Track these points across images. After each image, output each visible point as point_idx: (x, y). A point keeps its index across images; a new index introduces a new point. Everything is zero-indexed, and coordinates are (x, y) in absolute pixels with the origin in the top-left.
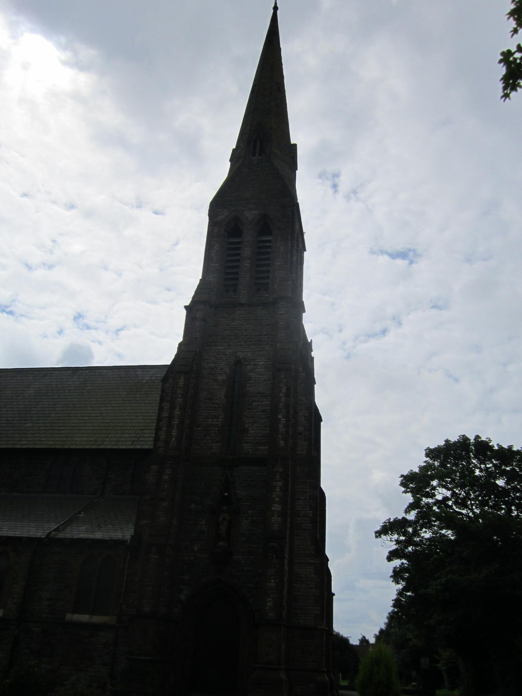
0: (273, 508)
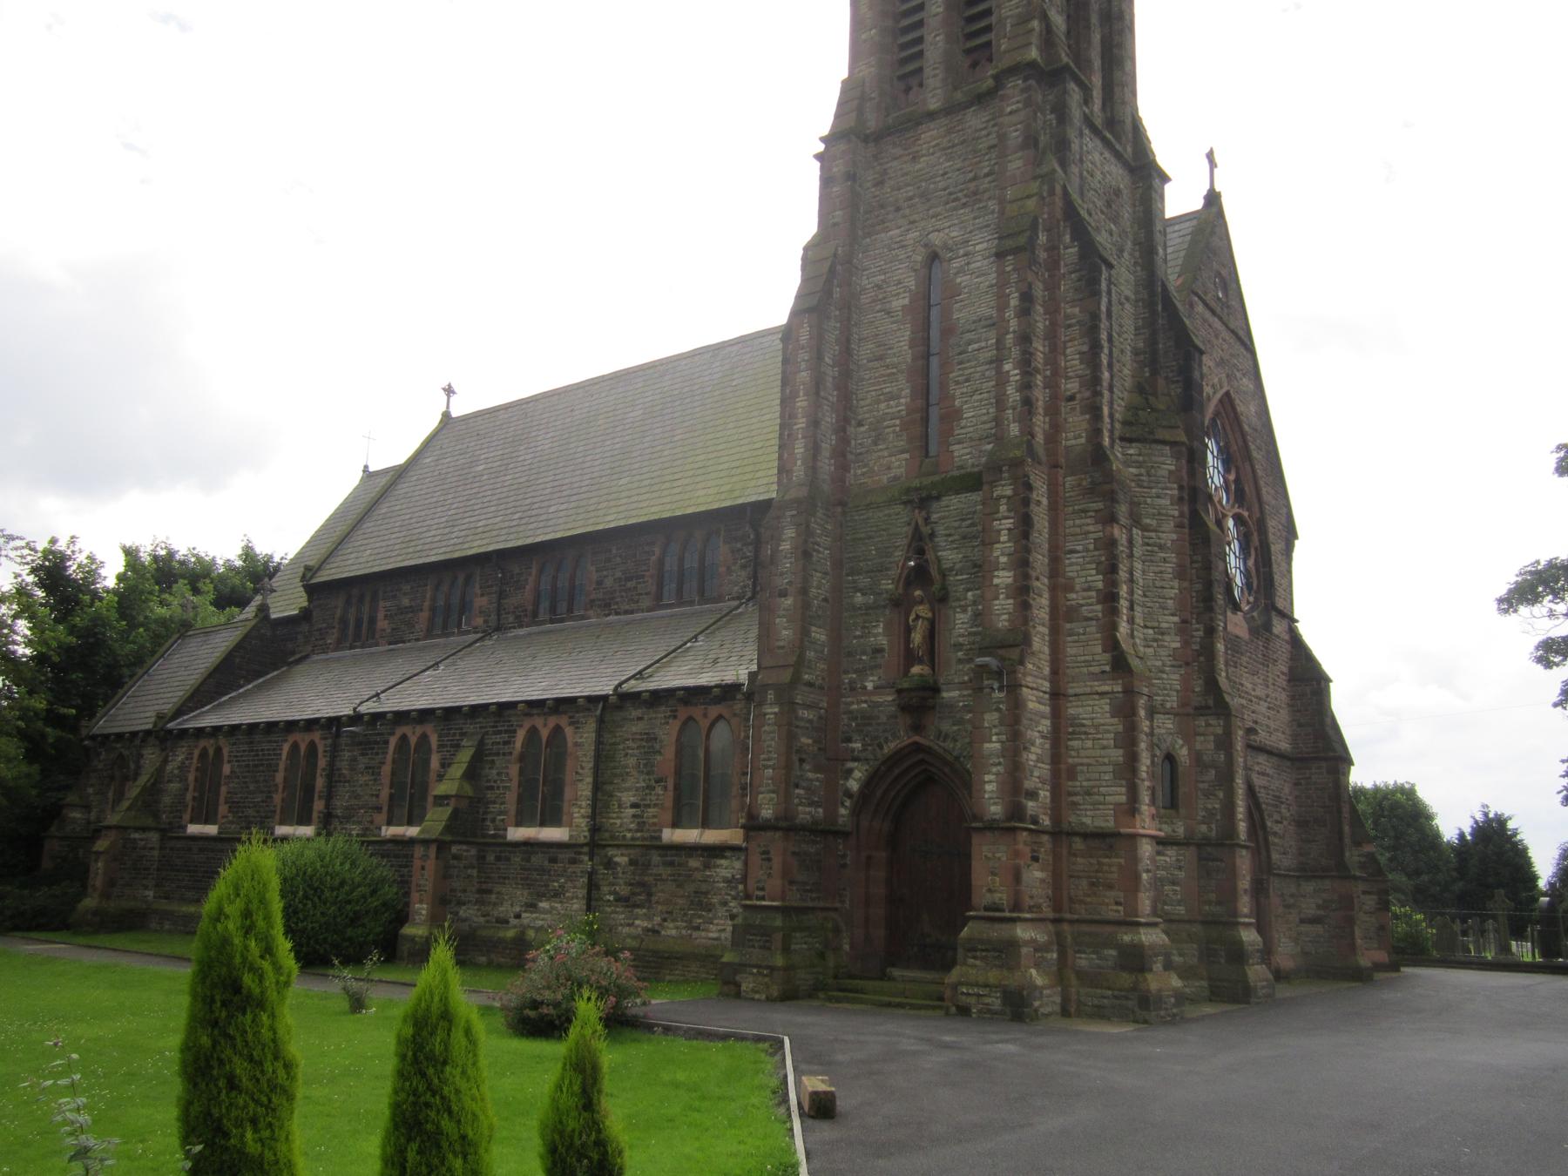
0: (996, 581)
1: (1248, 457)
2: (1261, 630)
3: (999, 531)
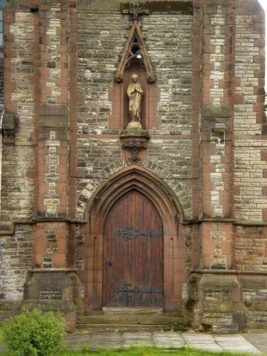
0: (212, 77)
3: (214, 46)
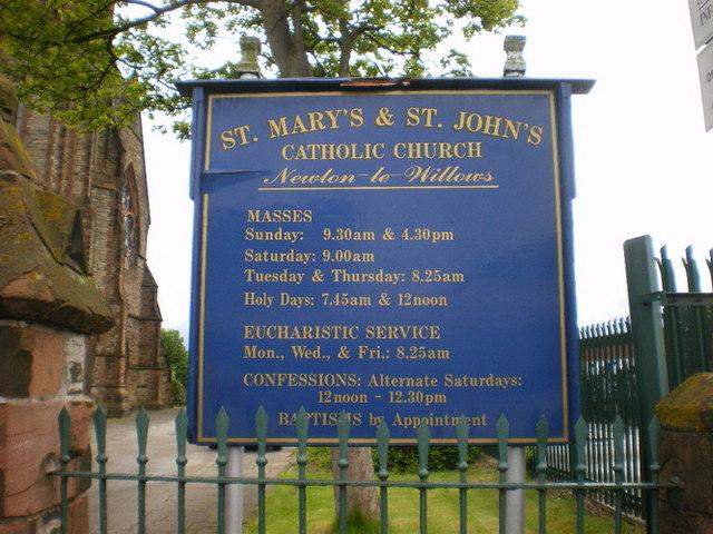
1: (136, 190)
2: (134, 265)
